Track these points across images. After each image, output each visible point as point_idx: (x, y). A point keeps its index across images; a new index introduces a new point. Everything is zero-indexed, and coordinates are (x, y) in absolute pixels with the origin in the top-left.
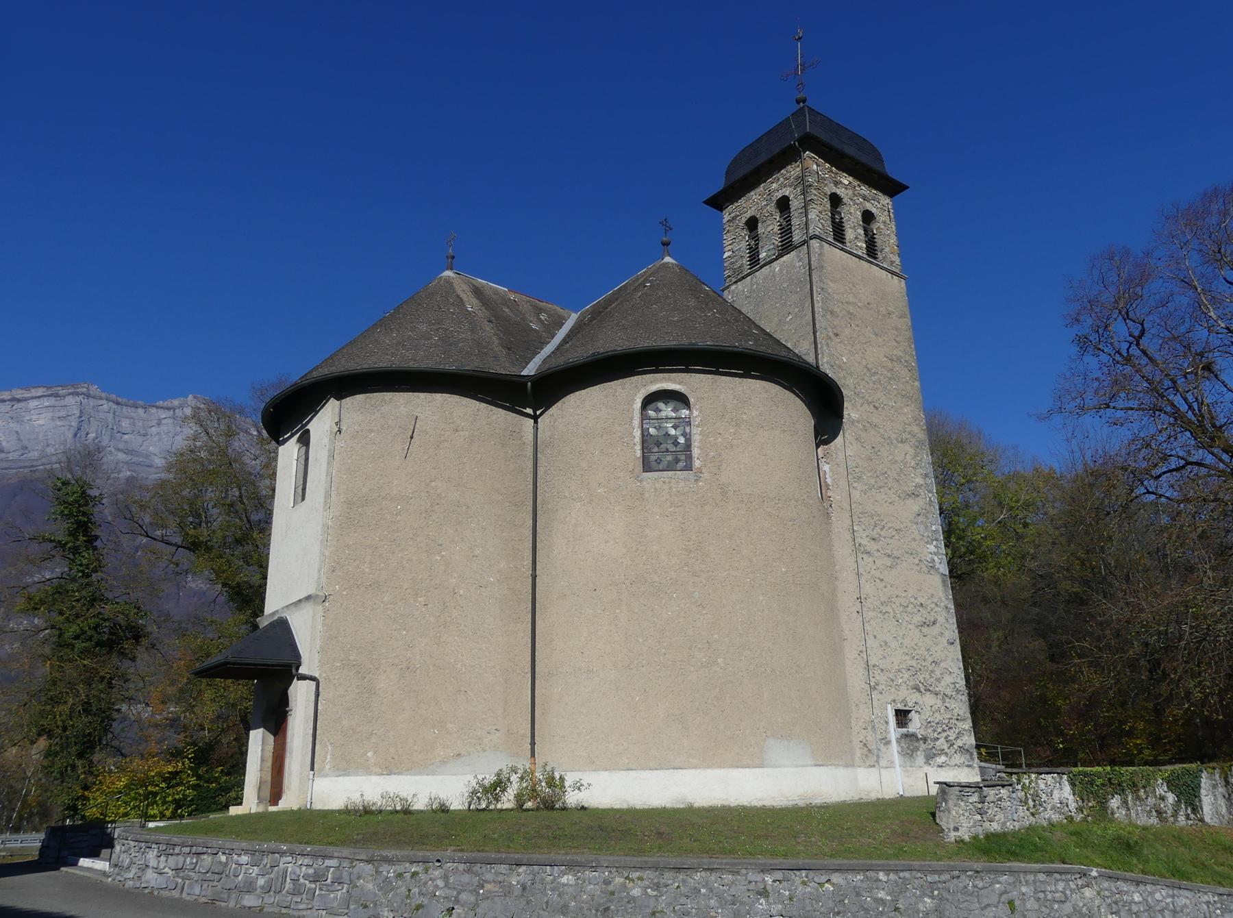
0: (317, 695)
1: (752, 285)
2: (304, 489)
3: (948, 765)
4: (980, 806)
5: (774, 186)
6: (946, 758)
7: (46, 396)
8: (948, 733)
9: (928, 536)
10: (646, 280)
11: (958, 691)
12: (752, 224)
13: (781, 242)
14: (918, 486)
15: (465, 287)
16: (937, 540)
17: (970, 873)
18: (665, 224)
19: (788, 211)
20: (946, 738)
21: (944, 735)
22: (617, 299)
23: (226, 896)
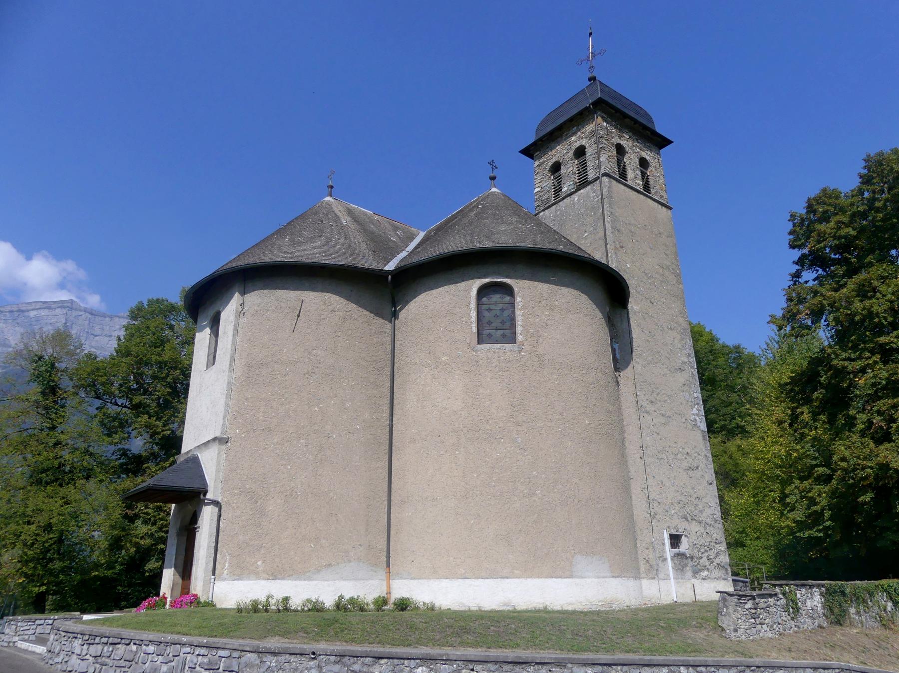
0: (220, 516)
1: (556, 211)
2: (214, 357)
3: (709, 578)
4: (753, 611)
5: (573, 138)
6: (707, 573)
7: (42, 308)
8: (709, 553)
9: (692, 401)
10: (479, 203)
11: (716, 521)
12: (556, 168)
13: (579, 179)
14: (684, 363)
15: (341, 208)
16: (698, 404)
17: (753, 668)
18: (492, 163)
19: (584, 156)
20: (708, 557)
21: (706, 554)
22: (456, 218)
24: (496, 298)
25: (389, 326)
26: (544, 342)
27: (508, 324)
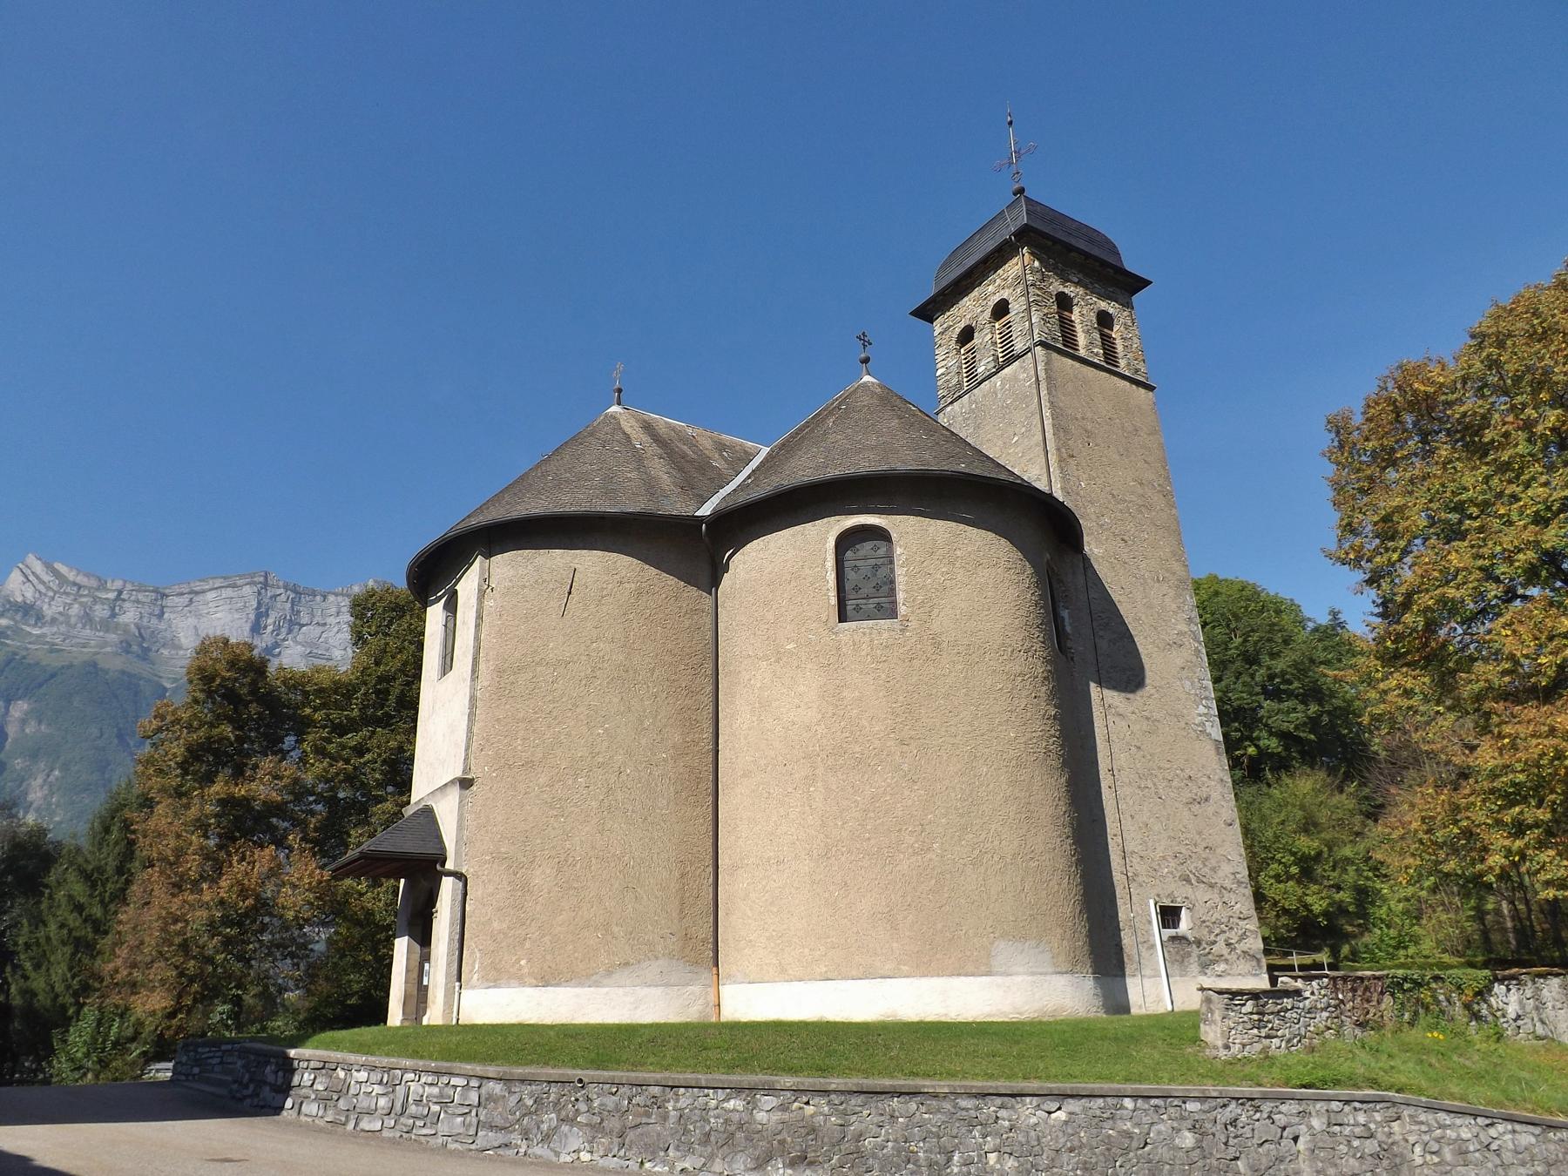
5: (991, 288)
7: (223, 587)
10: (840, 404)
11: (1239, 883)
23: (343, 1119)
24: (866, 548)
25: (707, 600)
26: (942, 614)
27: (885, 588)
